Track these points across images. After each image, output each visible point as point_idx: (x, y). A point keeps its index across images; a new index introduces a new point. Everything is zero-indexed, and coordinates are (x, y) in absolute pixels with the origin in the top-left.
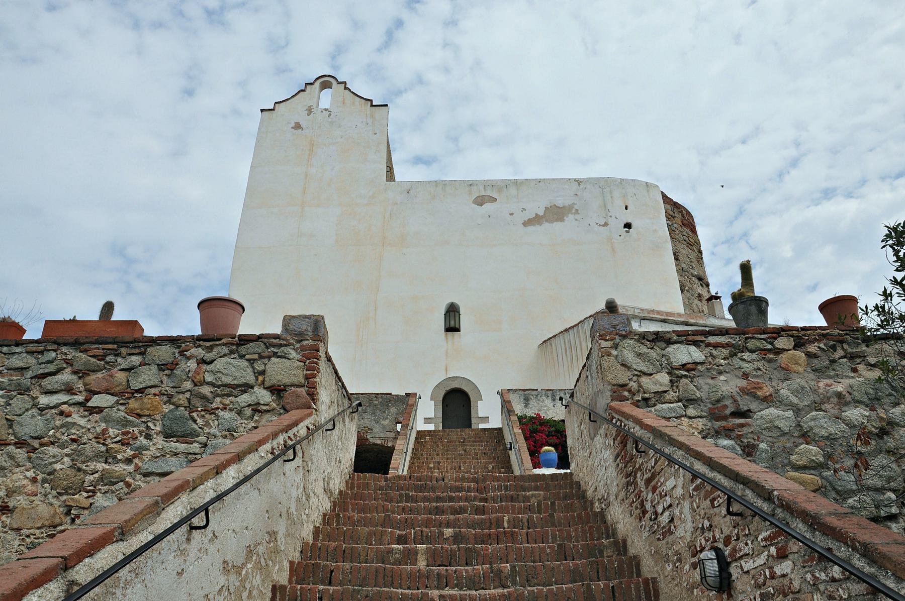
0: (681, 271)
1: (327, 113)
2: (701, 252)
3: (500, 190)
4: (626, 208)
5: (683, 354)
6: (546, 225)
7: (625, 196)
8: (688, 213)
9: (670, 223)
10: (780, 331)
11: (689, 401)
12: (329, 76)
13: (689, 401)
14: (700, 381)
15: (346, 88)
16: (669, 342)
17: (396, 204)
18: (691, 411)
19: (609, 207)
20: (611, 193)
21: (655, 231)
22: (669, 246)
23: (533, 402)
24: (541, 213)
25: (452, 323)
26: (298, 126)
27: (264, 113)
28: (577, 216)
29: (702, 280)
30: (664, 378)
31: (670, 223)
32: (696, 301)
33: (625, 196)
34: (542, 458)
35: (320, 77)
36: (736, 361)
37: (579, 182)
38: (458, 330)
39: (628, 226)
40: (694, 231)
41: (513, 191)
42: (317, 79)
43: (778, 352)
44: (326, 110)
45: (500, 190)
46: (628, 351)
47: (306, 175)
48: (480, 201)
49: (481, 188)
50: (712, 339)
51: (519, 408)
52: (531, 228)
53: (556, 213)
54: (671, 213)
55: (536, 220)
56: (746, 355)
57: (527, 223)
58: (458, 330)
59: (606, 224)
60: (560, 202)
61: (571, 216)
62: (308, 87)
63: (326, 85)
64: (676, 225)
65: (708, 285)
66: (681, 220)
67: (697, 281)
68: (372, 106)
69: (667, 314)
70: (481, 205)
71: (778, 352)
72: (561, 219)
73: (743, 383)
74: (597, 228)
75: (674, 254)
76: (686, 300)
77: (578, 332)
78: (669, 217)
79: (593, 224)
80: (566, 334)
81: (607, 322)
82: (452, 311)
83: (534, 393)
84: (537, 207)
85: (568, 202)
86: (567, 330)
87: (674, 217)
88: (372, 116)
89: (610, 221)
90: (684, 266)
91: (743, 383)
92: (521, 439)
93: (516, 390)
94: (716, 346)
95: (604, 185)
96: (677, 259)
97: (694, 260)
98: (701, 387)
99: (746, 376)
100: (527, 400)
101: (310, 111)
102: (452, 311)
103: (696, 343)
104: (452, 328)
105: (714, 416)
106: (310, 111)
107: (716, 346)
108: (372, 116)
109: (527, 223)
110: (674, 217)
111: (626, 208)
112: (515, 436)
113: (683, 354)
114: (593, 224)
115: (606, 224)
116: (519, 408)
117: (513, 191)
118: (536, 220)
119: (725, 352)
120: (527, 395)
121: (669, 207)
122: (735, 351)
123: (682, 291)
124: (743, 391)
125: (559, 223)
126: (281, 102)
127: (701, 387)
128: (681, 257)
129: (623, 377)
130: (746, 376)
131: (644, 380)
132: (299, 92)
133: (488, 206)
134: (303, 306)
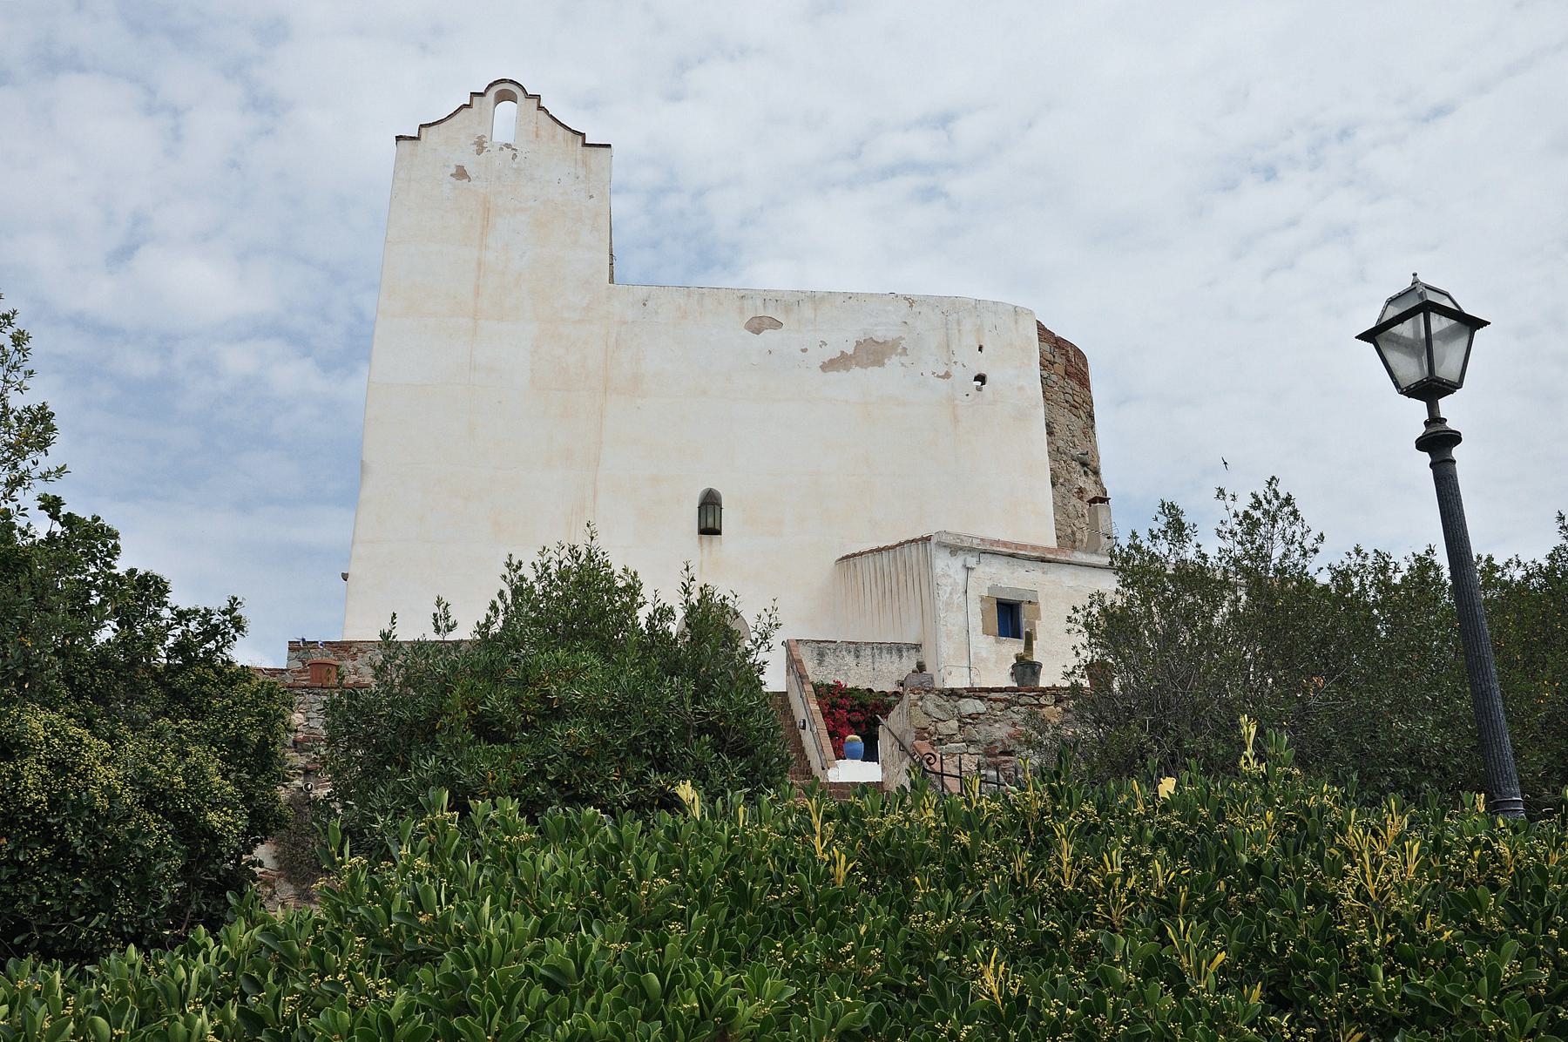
0: (1055, 453)
1: (509, 152)
2: (1091, 416)
3: (788, 309)
4: (980, 349)
5: (971, 706)
6: (856, 371)
7: (979, 330)
8: (1078, 352)
9: (1045, 374)
10: (1044, 691)
11: (972, 742)
12: (512, 82)
13: (972, 742)
14: (981, 727)
15: (540, 108)
16: (961, 696)
17: (625, 323)
18: (971, 750)
19: (953, 347)
20: (959, 322)
21: (1021, 388)
22: (1041, 412)
23: (829, 659)
24: (850, 351)
25: (710, 520)
26: (461, 173)
27: (401, 142)
28: (904, 359)
29: (1089, 466)
30: (954, 724)
31: (1045, 374)
32: (1075, 501)
33: (979, 330)
34: (846, 748)
35: (496, 82)
36: (1009, 713)
37: (911, 302)
38: (719, 533)
39: (981, 378)
40: (1084, 382)
41: (807, 311)
42: (491, 85)
43: (1042, 706)
44: (508, 146)
45: (788, 309)
46: (930, 703)
47: (479, 265)
48: (757, 326)
49: (759, 303)
50: (993, 695)
51: (810, 666)
52: (832, 375)
53: (872, 352)
54: (1050, 357)
55: (839, 363)
56: (1016, 708)
57: (828, 366)
58: (719, 533)
59: (947, 375)
60: (880, 334)
61: (895, 359)
62: (476, 99)
63: (503, 96)
64: (1054, 378)
65: (1096, 473)
66: (1065, 367)
67: (1079, 467)
68: (585, 145)
69: (1017, 546)
70: (758, 331)
71: (1042, 706)
72: (880, 363)
73: (1012, 730)
74: (933, 380)
75: (1047, 425)
76: (1059, 499)
77: (895, 558)
78: (1046, 364)
79: (928, 374)
80: (878, 556)
81: (915, 680)
82: (710, 503)
83: (832, 646)
84: (843, 340)
85: (891, 335)
86: (879, 550)
87: (1052, 363)
88: (585, 164)
89: (956, 371)
90: (1061, 443)
91: (1012, 730)
92: (819, 718)
93: (807, 642)
94: (995, 701)
95: (950, 310)
96: (1050, 433)
97: (1078, 433)
98: (981, 732)
99: (1014, 725)
100: (821, 655)
101: (480, 146)
102: (710, 503)
103: (981, 698)
104: (709, 529)
105: (987, 754)
106: (480, 146)
107: (995, 701)
108: (585, 164)
109: (828, 366)
110: (1052, 363)
111: (980, 349)
112: (806, 710)
113: (971, 706)
114: (928, 374)
115: (947, 375)
116: (817, 673)
117: (807, 311)
118: (839, 363)
119: (1002, 705)
120: (822, 649)
121: (1046, 347)
122: (1010, 704)
123: (1054, 485)
124: (1010, 736)
125: (876, 370)
126: (430, 125)
127: (981, 732)
128: (1057, 429)
129: (924, 722)
130: (1014, 725)
131: (940, 725)
132: (461, 108)
133: (768, 335)
134: (540, 541)
